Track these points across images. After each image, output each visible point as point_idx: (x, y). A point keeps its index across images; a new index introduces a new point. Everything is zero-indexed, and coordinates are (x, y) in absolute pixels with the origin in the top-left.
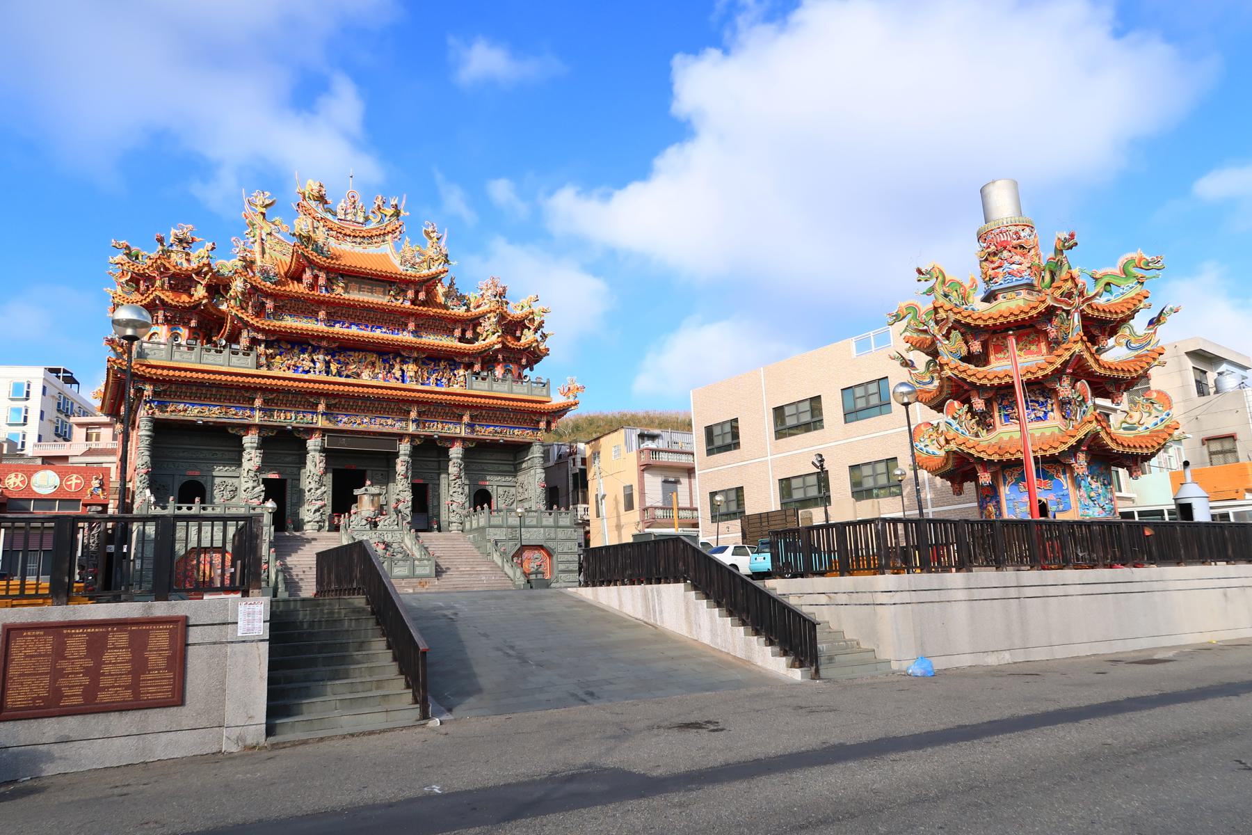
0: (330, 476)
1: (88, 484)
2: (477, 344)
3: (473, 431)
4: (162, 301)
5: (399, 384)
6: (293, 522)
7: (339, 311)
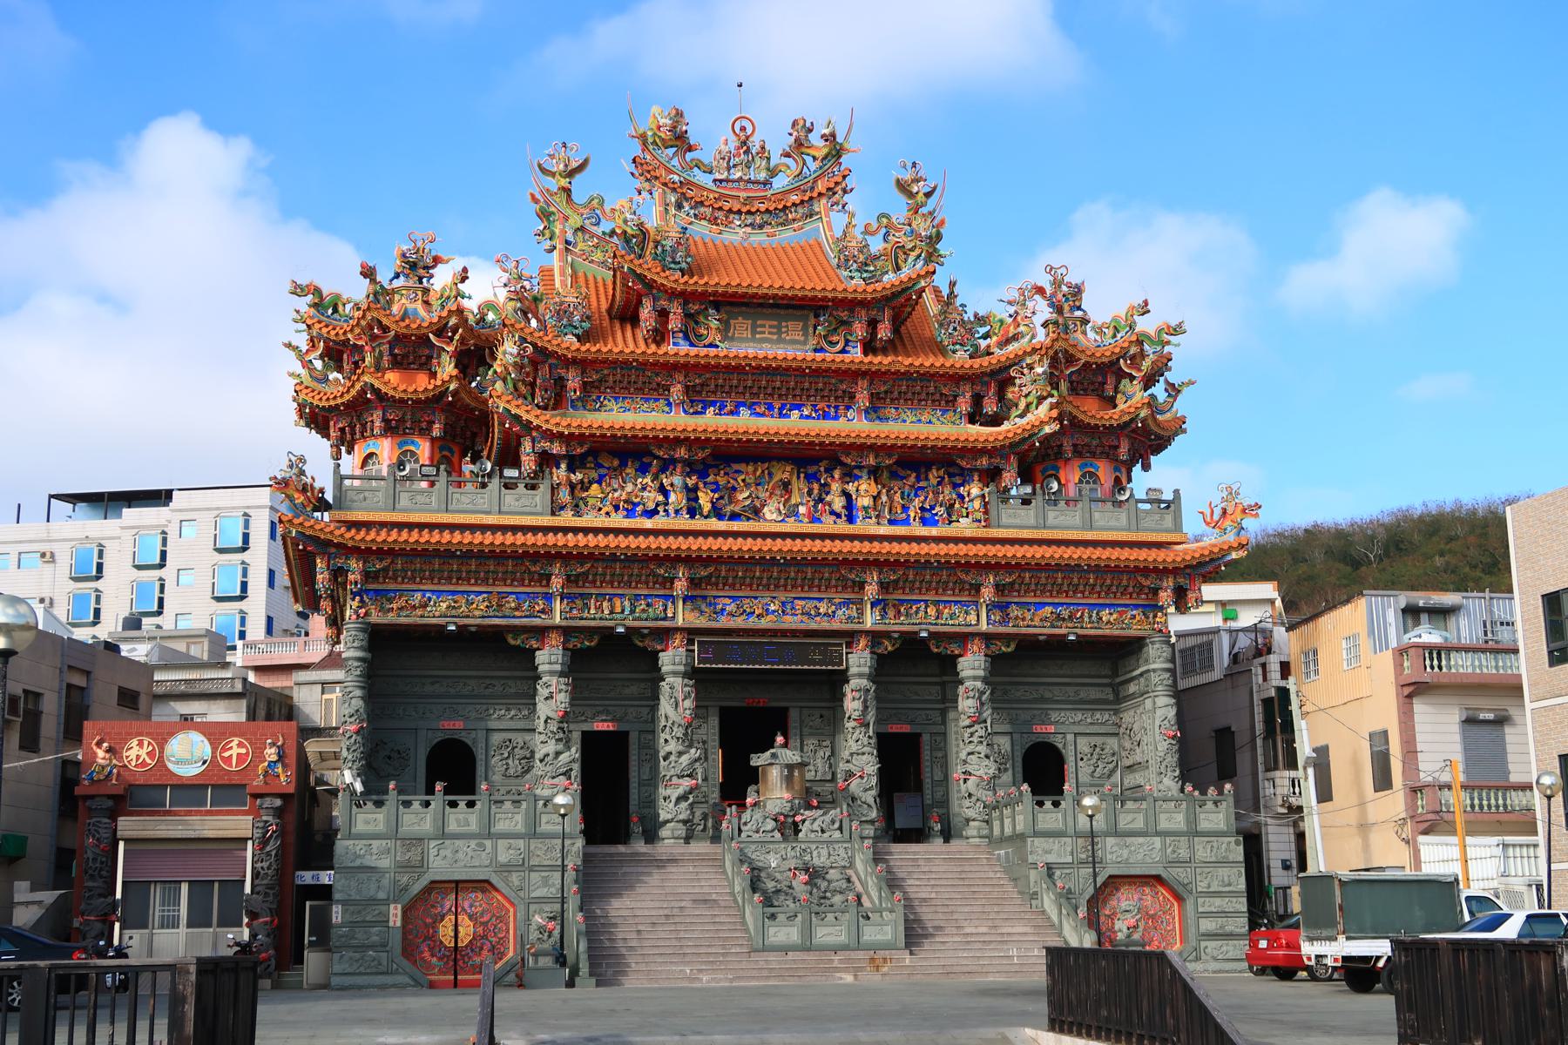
0: (714, 722)
1: (259, 755)
2: (1006, 426)
3: (1005, 620)
4: (376, 391)
5: (842, 527)
6: (642, 819)
7: (710, 383)
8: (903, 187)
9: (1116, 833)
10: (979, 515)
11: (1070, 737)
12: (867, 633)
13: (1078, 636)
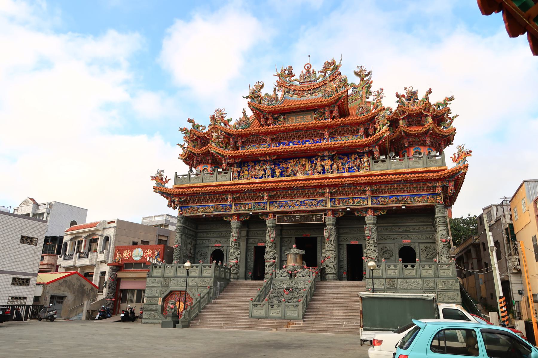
5: (321, 176)
8: (357, 74)
9: (404, 278)
10: (367, 168)
11: (417, 244)
12: (330, 210)
13: (406, 206)
